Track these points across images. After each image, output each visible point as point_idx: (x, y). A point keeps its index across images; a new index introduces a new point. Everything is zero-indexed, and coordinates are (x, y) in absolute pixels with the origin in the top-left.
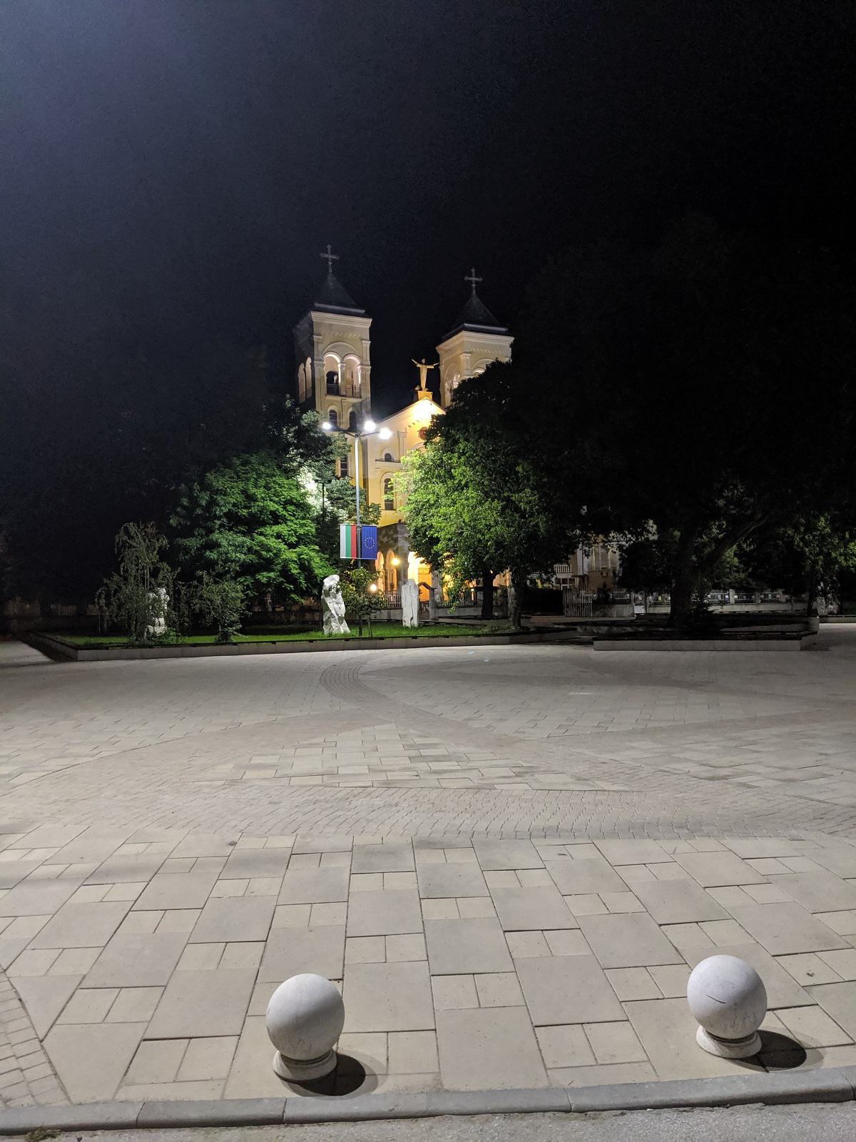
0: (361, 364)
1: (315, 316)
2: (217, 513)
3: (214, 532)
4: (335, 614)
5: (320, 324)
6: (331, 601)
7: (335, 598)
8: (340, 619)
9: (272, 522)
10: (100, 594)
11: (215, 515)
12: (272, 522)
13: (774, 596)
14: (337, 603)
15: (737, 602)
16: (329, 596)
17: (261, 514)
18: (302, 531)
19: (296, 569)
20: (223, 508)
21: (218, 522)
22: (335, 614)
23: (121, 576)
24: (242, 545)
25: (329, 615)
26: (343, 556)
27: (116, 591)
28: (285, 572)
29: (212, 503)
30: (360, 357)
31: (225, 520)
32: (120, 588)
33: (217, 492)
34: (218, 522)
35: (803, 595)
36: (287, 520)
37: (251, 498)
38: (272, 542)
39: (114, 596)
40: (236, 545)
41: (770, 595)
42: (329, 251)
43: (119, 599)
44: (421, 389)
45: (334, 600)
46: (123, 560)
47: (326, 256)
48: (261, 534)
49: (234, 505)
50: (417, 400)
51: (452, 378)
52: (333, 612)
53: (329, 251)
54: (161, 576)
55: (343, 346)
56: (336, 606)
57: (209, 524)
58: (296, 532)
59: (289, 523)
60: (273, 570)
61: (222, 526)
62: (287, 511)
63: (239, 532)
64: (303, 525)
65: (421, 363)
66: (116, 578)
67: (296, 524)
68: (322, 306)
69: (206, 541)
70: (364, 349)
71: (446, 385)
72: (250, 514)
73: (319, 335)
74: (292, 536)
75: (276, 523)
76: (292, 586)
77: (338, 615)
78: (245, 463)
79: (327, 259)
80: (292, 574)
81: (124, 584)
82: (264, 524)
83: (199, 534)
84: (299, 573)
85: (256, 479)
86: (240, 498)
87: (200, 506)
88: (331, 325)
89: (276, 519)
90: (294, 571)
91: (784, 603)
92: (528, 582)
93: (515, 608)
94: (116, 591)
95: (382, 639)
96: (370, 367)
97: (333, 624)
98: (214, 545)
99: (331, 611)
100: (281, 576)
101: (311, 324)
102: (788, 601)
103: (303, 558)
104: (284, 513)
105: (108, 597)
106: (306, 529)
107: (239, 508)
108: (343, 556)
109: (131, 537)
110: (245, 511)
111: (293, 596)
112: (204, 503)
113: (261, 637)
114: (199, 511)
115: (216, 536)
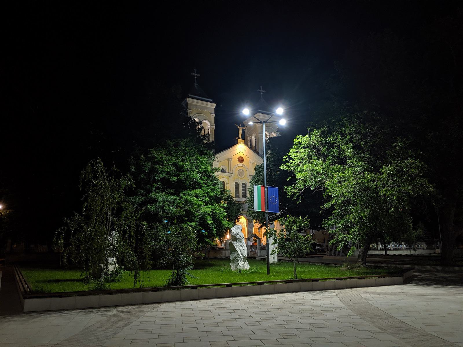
0: (210, 125)
1: (188, 100)
2: (156, 178)
3: (151, 192)
4: (241, 254)
5: (191, 104)
6: (237, 244)
7: (241, 242)
8: (244, 258)
9: (191, 187)
10: (60, 233)
11: (155, 179)
12: (191, 187)
13: (421, 246)
14: (242, 246)
15: (406, 249)
16: (236, 241)
17: (186, 180)
18: (212, 194)
19: (210, 220)
20: (160, 175)
21: (156, 185)
22: (241, 254)
23: (82, 215)
24: (173, 202)
25: (235, 255)
26: (256, 209)
27: (76, 231)
28: (203, 223)
29: (153, 171)
30: (210, 122)
31: (160, 184)
32: (81, 227)
33: (157, 163)
34: (156, 185)
35: (433, 246)
36: (201, 186)
37: (179, 169)
38: (194, 200)
39: (73, 237)
40: (169, 201)
41: (419, 245)
42: (196, 72)
43: (78, 239)
44: (239, 138)
45: (239, 243)
46: (86, 200)
47: (194, 74)
48: (184, 194)
49: (168, 173)
50: (237, 143)
51: (251, 136)
52: (239, 253)
53: (196, 72)
54: (123, 215)
55: (201, 115)
56: (241, 248)
57: (149, 187)
58: (208, 195)
59: (203, 188)
60: (193, 221)
61: (158, 188)
62: (203, 180)
63: (169, 193)
64: (213, 190)
65: (239, 126)
66: (77, 217)
67: (208, 189)
68: (192, 96)
69: (145, 199)
70: (212, 118)
71: (248, 139)
72: (179, 180)
73: (190, 109)
74: (206, 197)
75: (195, 188)
76: (207, 233)
77: (243, 255)
78: (175, 146)
79: (194, 76)
80: (208, 224)
81: (87, 223)
82: (186, 189)
83: (141, 194)
84: (212, 223)
85: (183, 156)
86: (172, 169)
87: (144, 172)
88: (196, 105)
89: (195, 185)
90: (209, 222)
91: (425, 250)
92: (119, 244)
93: (362, 252)
94: (76, 231)
95: (317, 280)
96: (215, 127)
97: (239, 262)
98: (154, 201)
99: (237, 252)
100: (200, 225)
101: (187, 104)
102: (427, 249)
103: (216, 212)
104: (200, 181)
105: (66, 238)
106: (215, 192)
107: (171, 176)
108: (256, 209)
109: (96, 177)
110: (175, 178)
111: (207, 240)
112: (147, 170)
113: (318, 303)
114: (143, 176)
115: (154, 194)
